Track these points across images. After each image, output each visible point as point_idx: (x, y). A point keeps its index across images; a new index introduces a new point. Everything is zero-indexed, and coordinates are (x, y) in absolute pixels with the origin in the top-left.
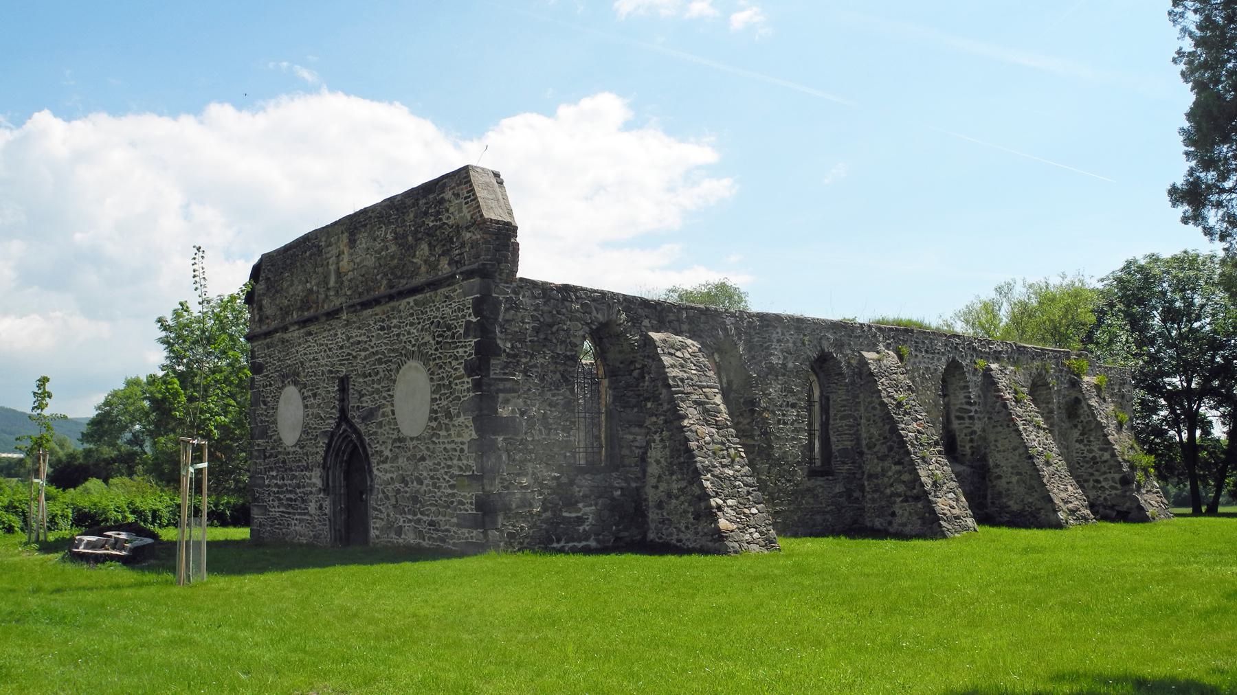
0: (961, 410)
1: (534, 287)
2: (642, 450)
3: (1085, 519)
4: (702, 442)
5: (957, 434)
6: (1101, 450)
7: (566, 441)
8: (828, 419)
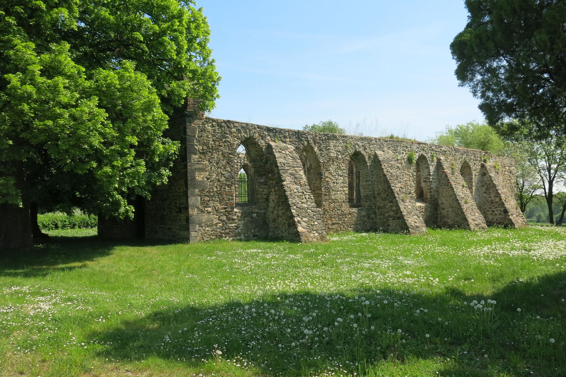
0: (426, 178)
1: (213, 122)
2: (267, 196)
3: (483, 228)
4: (292, 192)
5: (424, 189)
6: (495, 197)
7: (230, 192)
8: (359, 182)
